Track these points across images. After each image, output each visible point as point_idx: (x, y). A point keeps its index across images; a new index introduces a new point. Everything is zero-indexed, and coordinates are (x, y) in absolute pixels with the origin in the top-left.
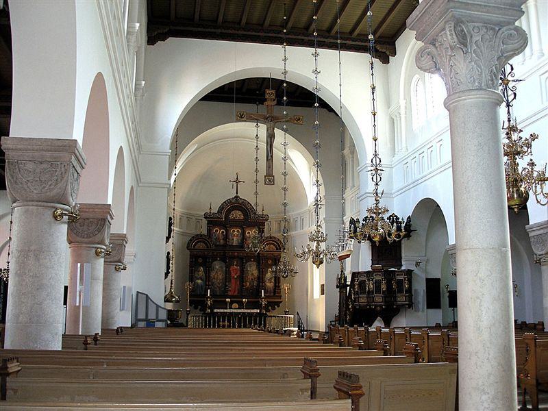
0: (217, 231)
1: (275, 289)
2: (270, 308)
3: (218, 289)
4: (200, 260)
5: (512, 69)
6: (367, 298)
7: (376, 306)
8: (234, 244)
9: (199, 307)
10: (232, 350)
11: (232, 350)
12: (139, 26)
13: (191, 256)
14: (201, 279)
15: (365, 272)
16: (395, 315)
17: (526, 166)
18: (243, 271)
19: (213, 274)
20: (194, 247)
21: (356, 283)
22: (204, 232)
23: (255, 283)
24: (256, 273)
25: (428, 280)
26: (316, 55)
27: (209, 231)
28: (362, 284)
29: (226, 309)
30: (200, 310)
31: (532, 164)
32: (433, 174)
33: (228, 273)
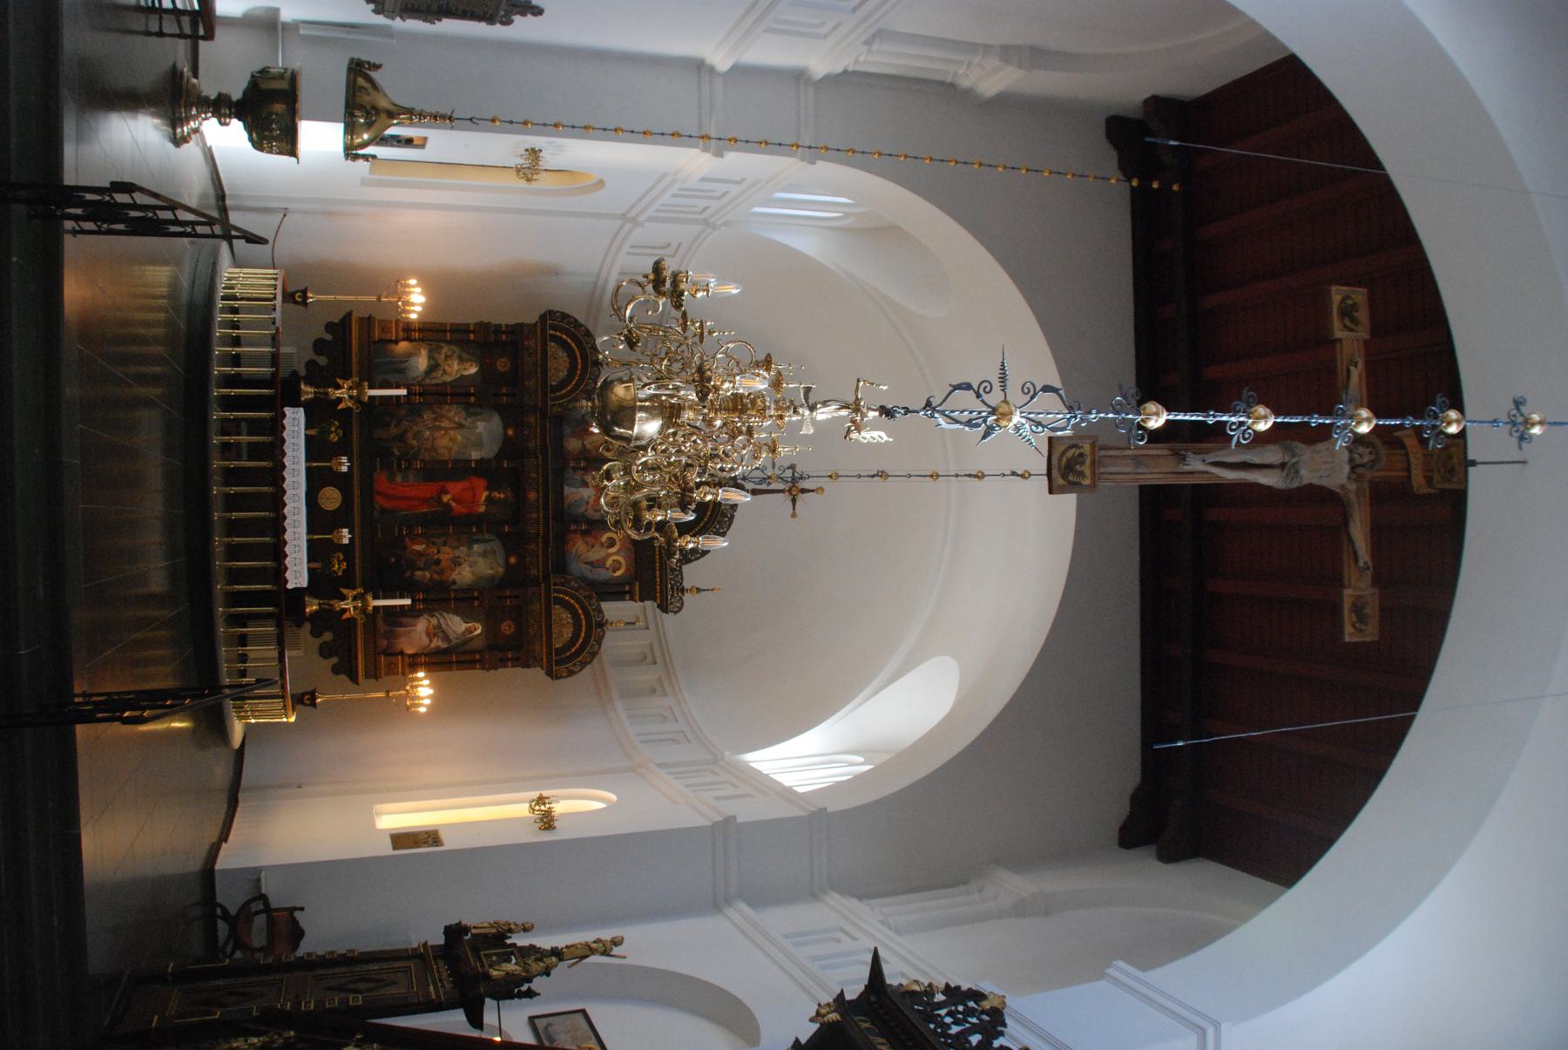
2: (328, 636)
3: (393, 431)
5: (968, 387)
8: (568, 490)
12: (1119, 809)
14: (433, 368)
16: (1184, 859)
18: (465, 527)
19: (454, 413)
20: (554, 338)
23: (423, 575)
24: (464, 575)
26: (866, 963)
33: (461, 469)
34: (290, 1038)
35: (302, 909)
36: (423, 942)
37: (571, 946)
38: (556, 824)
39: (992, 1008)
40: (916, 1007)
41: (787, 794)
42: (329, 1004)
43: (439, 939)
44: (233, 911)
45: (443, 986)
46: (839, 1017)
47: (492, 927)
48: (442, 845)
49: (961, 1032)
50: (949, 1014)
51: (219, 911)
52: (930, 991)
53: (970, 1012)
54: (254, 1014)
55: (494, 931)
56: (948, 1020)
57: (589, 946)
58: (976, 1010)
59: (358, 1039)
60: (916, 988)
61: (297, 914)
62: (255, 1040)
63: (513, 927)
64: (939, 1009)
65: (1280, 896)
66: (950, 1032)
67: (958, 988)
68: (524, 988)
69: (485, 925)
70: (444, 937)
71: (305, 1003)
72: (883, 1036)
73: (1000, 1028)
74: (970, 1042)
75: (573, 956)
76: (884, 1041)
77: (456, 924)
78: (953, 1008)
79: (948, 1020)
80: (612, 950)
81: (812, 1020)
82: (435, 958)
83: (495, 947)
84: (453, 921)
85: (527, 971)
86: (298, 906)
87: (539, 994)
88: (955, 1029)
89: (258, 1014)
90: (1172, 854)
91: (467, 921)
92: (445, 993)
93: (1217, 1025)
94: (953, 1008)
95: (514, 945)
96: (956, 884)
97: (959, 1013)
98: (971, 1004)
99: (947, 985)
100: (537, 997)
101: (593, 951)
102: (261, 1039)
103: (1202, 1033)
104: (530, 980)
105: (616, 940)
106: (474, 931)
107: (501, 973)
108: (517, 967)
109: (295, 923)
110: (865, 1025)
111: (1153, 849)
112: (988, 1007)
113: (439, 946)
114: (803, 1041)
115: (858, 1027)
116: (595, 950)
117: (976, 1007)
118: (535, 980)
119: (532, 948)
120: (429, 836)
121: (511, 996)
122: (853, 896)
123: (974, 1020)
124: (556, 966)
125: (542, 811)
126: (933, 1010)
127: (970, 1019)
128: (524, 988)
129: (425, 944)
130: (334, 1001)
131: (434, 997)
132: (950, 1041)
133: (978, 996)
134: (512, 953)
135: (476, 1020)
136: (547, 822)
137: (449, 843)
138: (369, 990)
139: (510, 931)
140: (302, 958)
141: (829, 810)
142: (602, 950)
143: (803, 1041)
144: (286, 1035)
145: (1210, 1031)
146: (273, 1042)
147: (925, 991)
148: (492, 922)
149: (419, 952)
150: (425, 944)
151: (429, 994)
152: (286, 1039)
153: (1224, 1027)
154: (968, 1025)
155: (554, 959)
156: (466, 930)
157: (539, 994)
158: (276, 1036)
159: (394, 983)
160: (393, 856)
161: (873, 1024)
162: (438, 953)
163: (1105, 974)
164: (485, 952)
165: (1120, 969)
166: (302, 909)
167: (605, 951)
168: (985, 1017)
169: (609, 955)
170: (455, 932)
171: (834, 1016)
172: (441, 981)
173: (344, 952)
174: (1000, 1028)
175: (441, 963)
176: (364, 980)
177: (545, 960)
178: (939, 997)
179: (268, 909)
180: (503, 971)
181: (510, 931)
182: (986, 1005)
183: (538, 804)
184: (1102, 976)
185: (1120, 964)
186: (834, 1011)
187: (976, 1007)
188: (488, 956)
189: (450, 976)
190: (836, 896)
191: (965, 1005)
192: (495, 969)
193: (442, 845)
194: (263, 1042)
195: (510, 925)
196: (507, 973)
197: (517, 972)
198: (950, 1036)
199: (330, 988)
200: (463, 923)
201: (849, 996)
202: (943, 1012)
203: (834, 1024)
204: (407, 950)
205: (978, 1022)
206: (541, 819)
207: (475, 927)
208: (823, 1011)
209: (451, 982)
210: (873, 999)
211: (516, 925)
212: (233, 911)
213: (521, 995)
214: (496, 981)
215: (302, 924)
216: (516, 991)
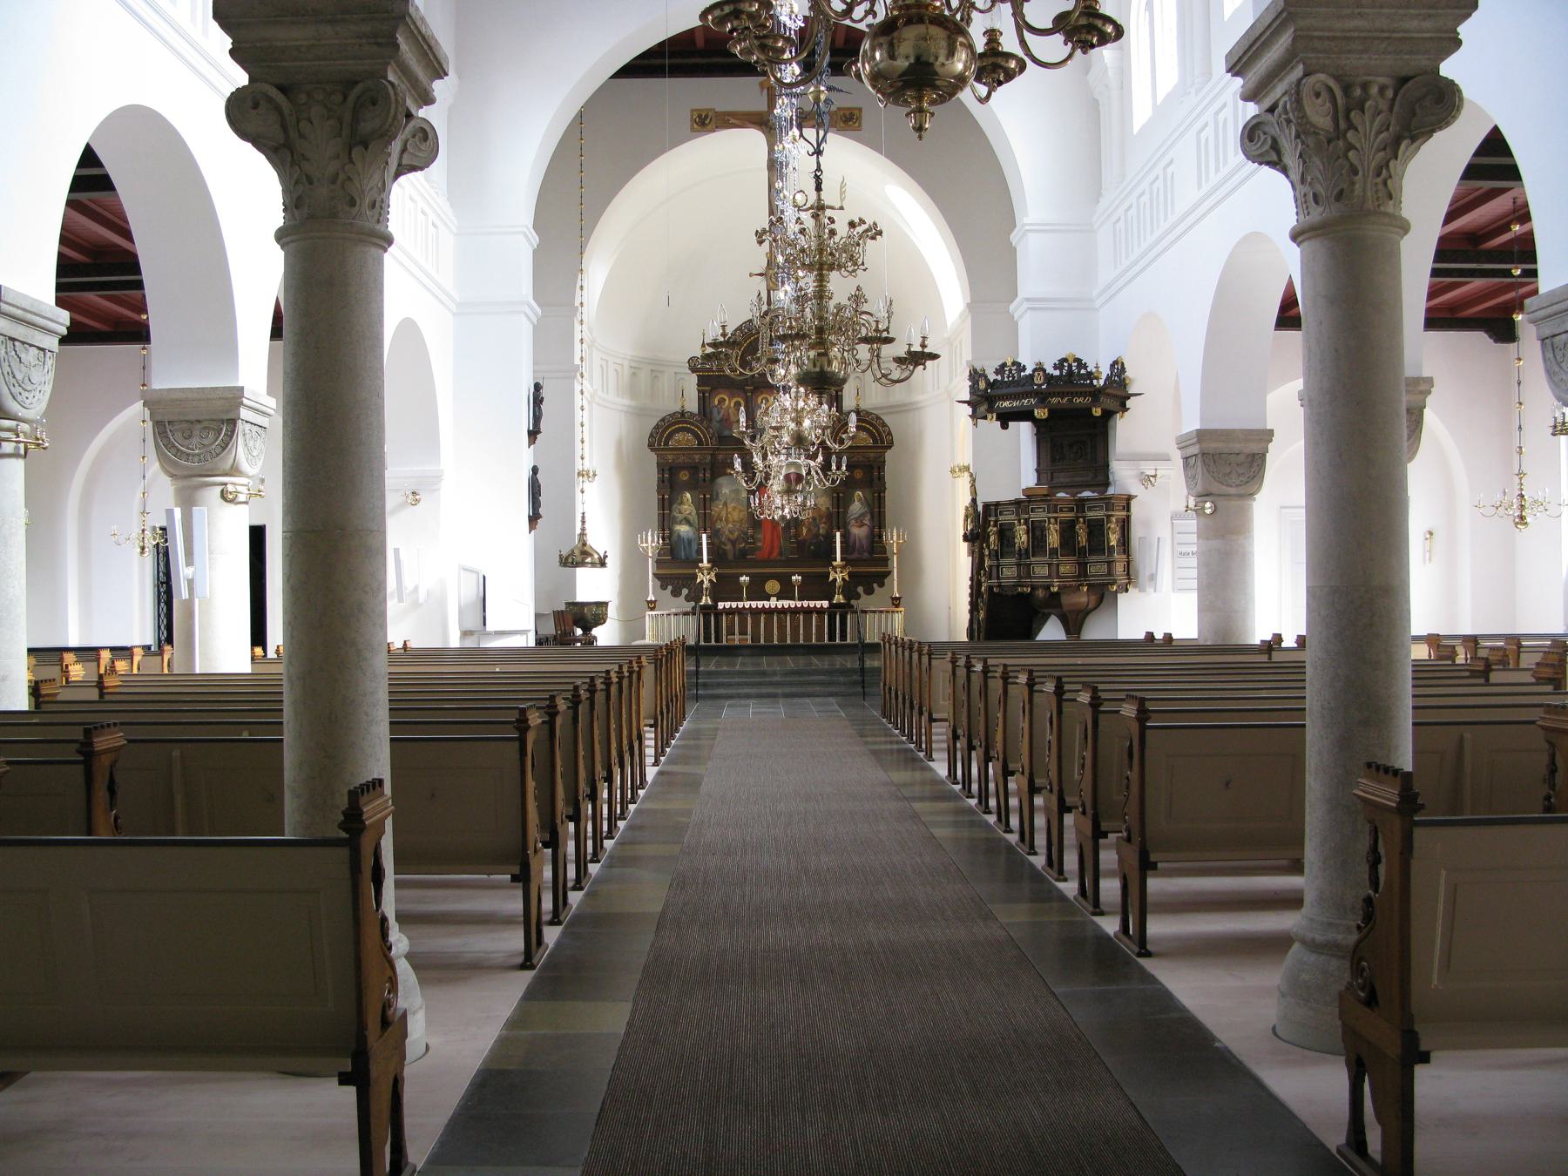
0: (722, 401)
1: (873, 542)
2: (860, 589)
3: (729, 547)
4: (684, 476)
6: (1018, 565)
7: (1034, 588)
9: (685, 591)
10: (904, 703)
11: (904, 703)
13: (661, 468)
14: (688, 522)
15: (1010, 503)
17: (845, 302)
19: (717, 508)
21: (992, 529)
22: (692, 406)
25: (395, 549)
27: (703, 400)
28: (1005, 534)
29: (741, 600)
30: (688, 599)
31: (858, 298)
32: (1164, 243)
145: (1027, 228)
185: (1011, 237)
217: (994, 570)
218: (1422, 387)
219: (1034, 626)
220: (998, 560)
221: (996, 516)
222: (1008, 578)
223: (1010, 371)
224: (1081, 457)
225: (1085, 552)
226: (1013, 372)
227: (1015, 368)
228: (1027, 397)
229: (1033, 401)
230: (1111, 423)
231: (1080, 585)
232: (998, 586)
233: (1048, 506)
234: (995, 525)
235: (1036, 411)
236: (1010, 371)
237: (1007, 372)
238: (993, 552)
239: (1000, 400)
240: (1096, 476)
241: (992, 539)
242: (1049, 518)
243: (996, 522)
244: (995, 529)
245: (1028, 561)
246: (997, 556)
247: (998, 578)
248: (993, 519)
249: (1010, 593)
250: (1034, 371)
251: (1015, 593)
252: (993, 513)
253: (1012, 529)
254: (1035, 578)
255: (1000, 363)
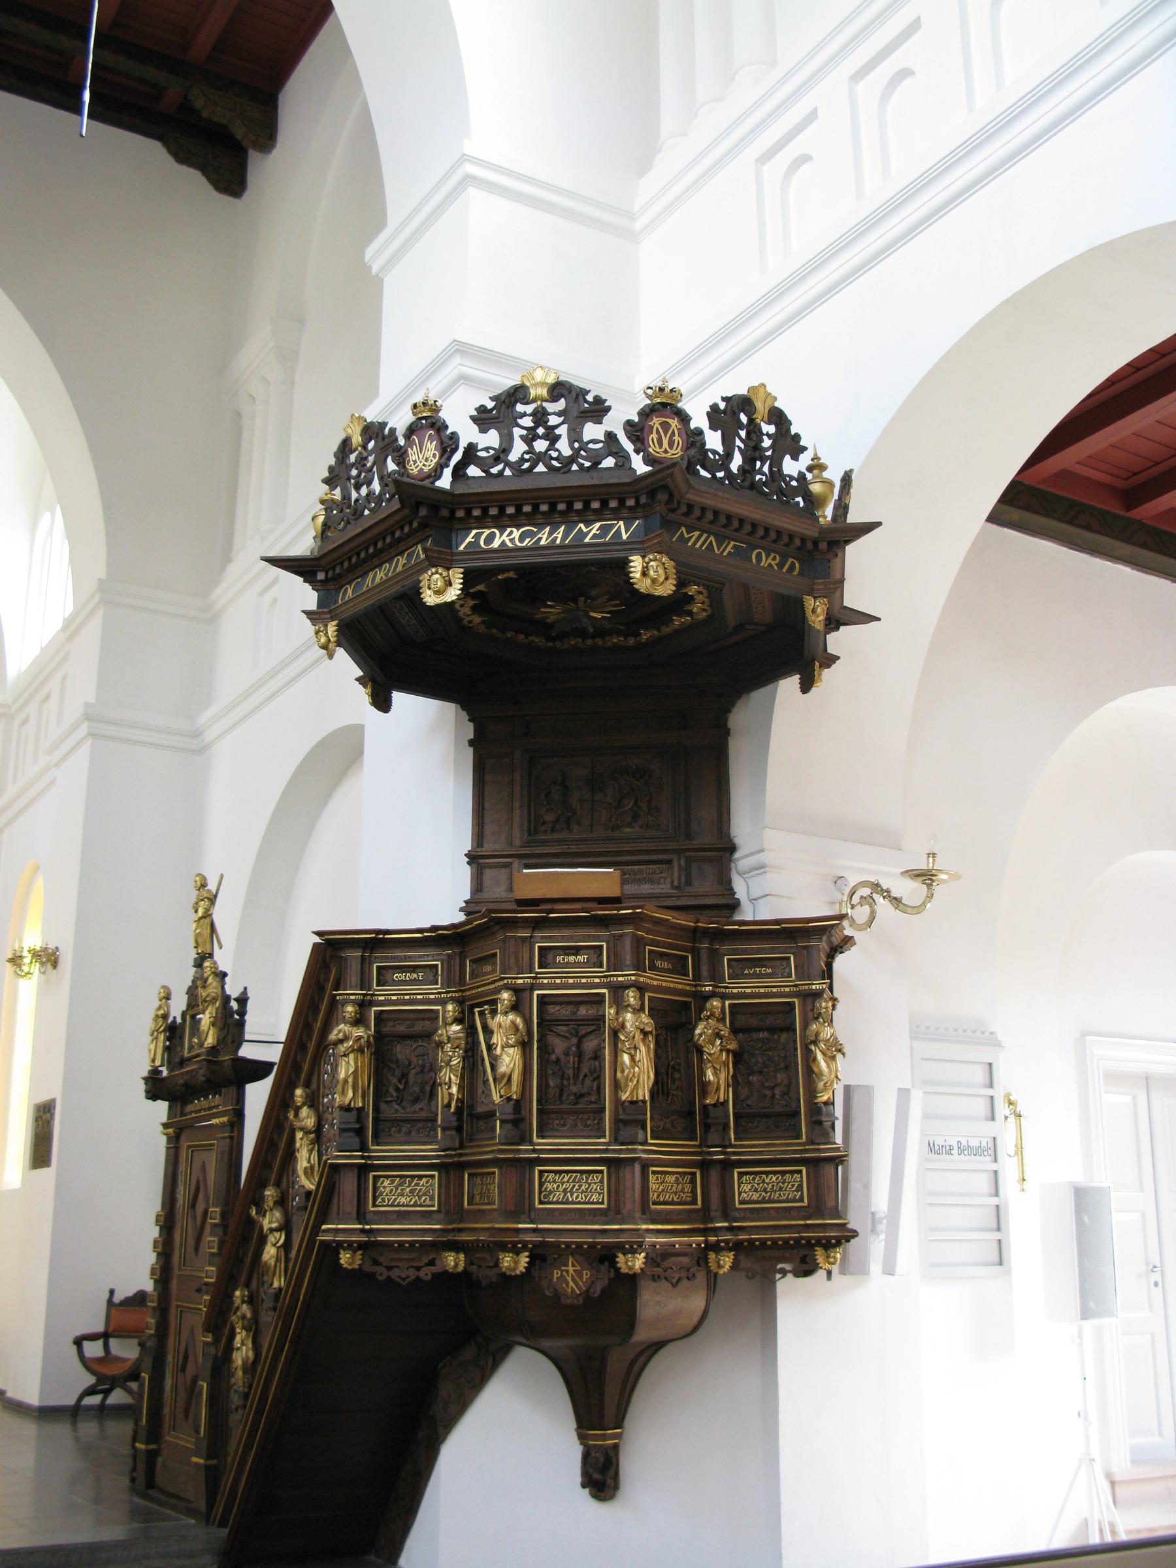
7: (542, 1255)
12: (192, 180)
34: (243, 1296)
35: (112, 1292)
36: (161, 1128)
37: (197, 942)
38: (52, 946)
39: (361, 435)
40: (745, 546)
41: (72, 628)
42: (213, 1248)
43: (162, 1106)
44: (90, 1380)
45: (217, 1106)
46: (334, 623)
47: (156, 1038)
48: (54, 1101)
49: (381, 478)
50: (358, 488)
51: (95, 1400)
52: (328, 504)
53: (362, 460)
54: (209, 1340)
55: (162, 1037)
56: (364, 491)
57: (200, 918)
58: (360, 453)
59: (257, 1213)
60: (321, 519)
61: (117, 1299)
62: (238, 1338)
63: (161, 1012)
64: (350, 499)
65: (338, 19)
66: (377, 493)
67: (331, 469)
68: (234, 1005)
69: (153, 1047)
70: (159, 1102)
71: (207, 1278)
72: (365, 574)
73: (387, 431)
74: (394, 472)
75: (208, 940)
76: (371, 575)
77: (146, 1084)
78: (352, 481)
79: (364, 491)
80: (209, 891)
81: (331, 656)
82: (183, 1114)
83: (182, 1038)
84: (141, 1087)
85: (214, 999)
86: (107, 1295)
87: (245, 988)
88: (376, 486)
89: (211, 1335)
90: (266, 135)
91: (145, 1070)
92: (225, 1105)
93: (465, 158)
94: (352, 481)
95: (184, 1014)
96: (237, 431)
97: (359, 475)
98: (353, 458)
99: (326, 481)
100: (249, 991)
101: (207, 915)
102: (238, 1330)
103: (469, 180)
104: (226, 999)
105: (199, 883)
106: (158, 1063)
107: (211, 1033)
108: (207, 1012)
109: (129, 1302)
110: (350, 591)
111: (253, 156)
112: (360, 439)
113: (170, 1108)
114: (360, 673)
115: (351, 600)
116: (205, 912)
117: (357, 452)
118: (228, 992)
119: (192, 992)
120: (41, 1117)
121: (241, 1024)
122: (222, 569)
123: (371, 459)
124: (215, 963)
125: (31, 962)
126: (349, 507)
127: (369, 465)
128: (234, 1005)
129: (165, 1126)
130: (211, 1241)
131: (225, 1119)
132: (387, 496)
133: (345, 447)
134: (193, 1017)
135: (258, 1070)
136: (49, 958)
137: (52, 1091)
138: (207, 1198)
139: (165, 1017)
140: (156, 1282)
141: (103, 576)
142: (206, 903)
143: (360, 673)
144: (238, 1301)
145: (470, 169)
146: (244, 1317)
147: (326, 510)
148: (151, 1038)
149: (173, 1135)
150: (165, 1126)
151: (222, 1125)
152: (243, 1302)
153: (469, 149)
154: (375, 469)
155: (207, 964)
156: (155, 1072)
157: (245, 988)
158: (239, 1313)
159: (204, 1168)
160: (58, 1169)
161: (350, 583)
162: (179, 1111)
163: (377, 275)
164: (186, 1051)
165: (376, 254)
166: (112, 1292)
167: (209, 899)
168: (371, 445)
169: (216, 896)
170: (156, 1087)
171: (332, 628)
172: (210, 1108)
173: (158, 1228)
174: (387, 431)
175: (189, 1108)
176: (193, 1205)
177: (205, 975)
178: (337, 494)
179: (105, 1336)
180: (209, 1029)
181: (165, 1017)
182: (357, 439)
183: (19, 966)
184: (378, 282)
185: (369, 252)
186: (326, 626)
187: (357, 452)
188: (191, 1048)
189: (206, 1097)
190: (217, 592)
191: (353, 465)
192: (206, 1039)
193: (54, 1101)
194: (242, 1329)
195: (157, 1016)
196: (213, 1025)
197: (214, 1011)
198: (382, 493)
199: (197, 1248)
200: (146, 1074)
201: (312, 605)
202: (354, 495)
203: (340, 629)
204: (168, 1148)
205: (374, 455)
206: (42, 964)
207: (153, 1061)
208: (323, 640)
209: (214, 1096)
210: (321, 576)
211: (159, 1008)
212: (90, 1380)
213: (242, 1012)
214: (221, 1041)
215: (130, 1292)
216: (236, 1017)
217: (348, 1184)
218: (150, 1095)
219: (445, 1389)
220: (363, 1147)
221: (364, 984)
222: (402, 1216)
223: (540, 417)
224: (636, 817)
225: (726, 1127)
226: (553, 420)
227: (561, 404)
228: (599, 515)
229: (623, 530)
230: (740, 717)
231: (711, 1247)
232: (362, 1246)
233: (614, 942)
234: (359, 1021)
235: (637, 563)
236: (540, 417)
237: (527, 422)
238: (335, 1119)
239: (481, 523)
240: (689, 882)
241: (346, 1068)
242: (618, 990)
243: (363, 1005)
244: (359, 1032)
245: (524, 1151)
246: (360, 1132)
247: (361, 1215)
248: (354, 993)
249: (403, 1273)
250: (646, 413)
251: (426, 1273)
252: (353, 975)
253: (428, 1035)
254: (550, 1216)
255: (509, 381)
